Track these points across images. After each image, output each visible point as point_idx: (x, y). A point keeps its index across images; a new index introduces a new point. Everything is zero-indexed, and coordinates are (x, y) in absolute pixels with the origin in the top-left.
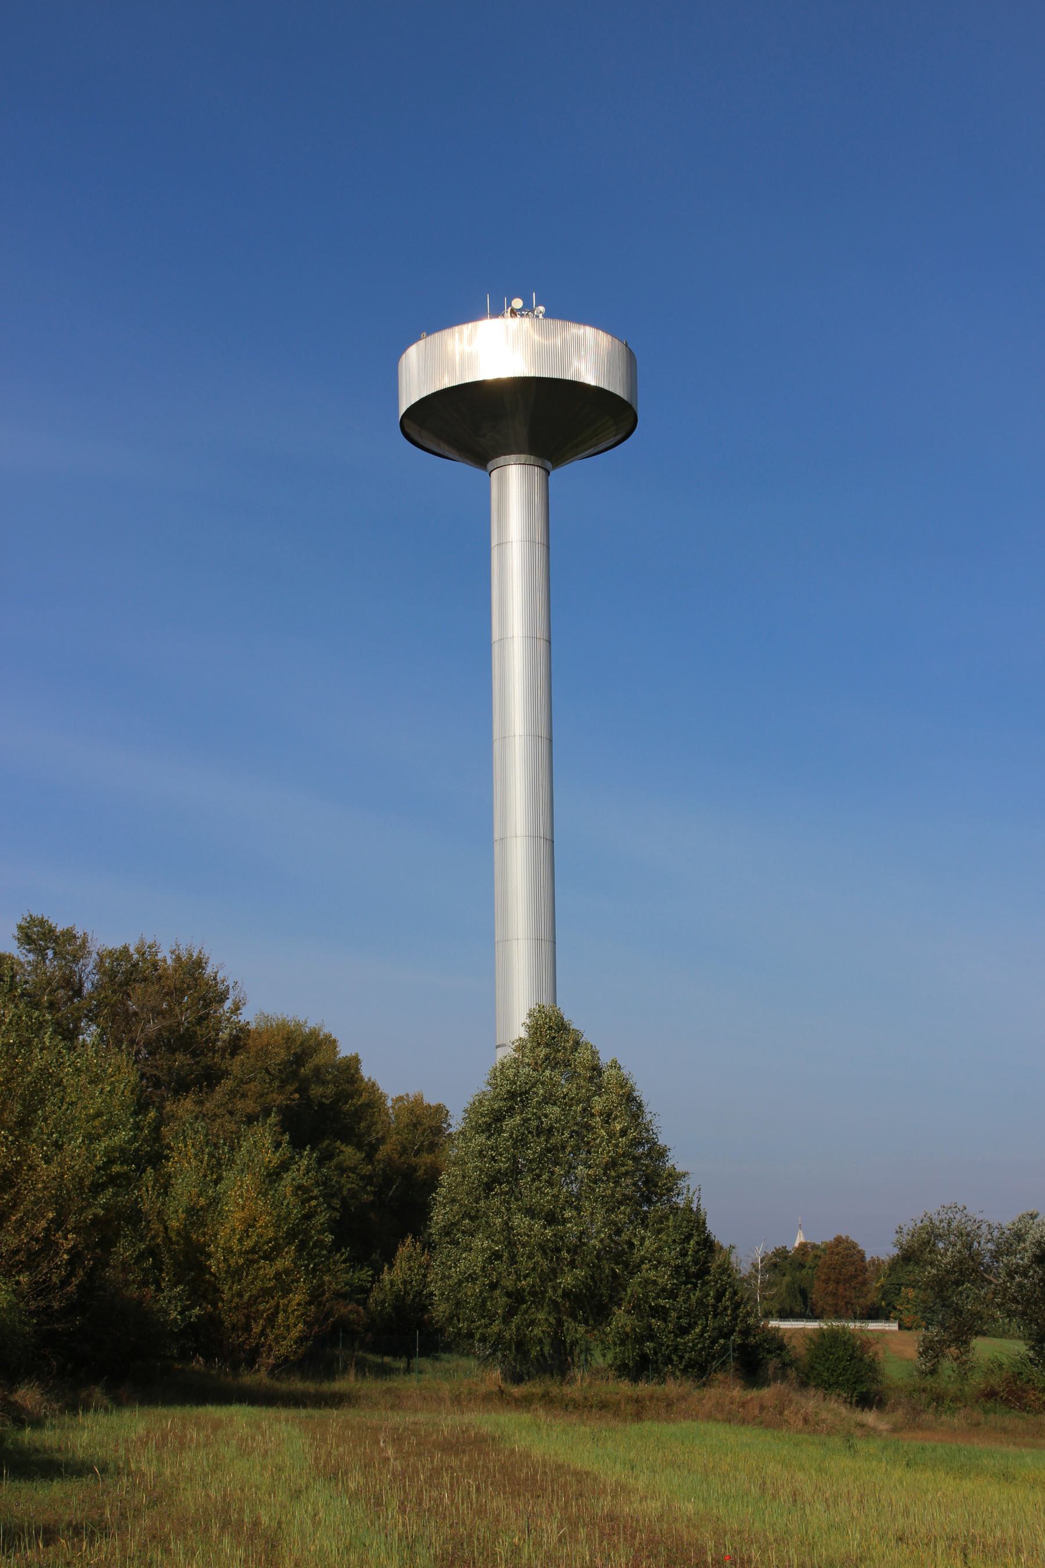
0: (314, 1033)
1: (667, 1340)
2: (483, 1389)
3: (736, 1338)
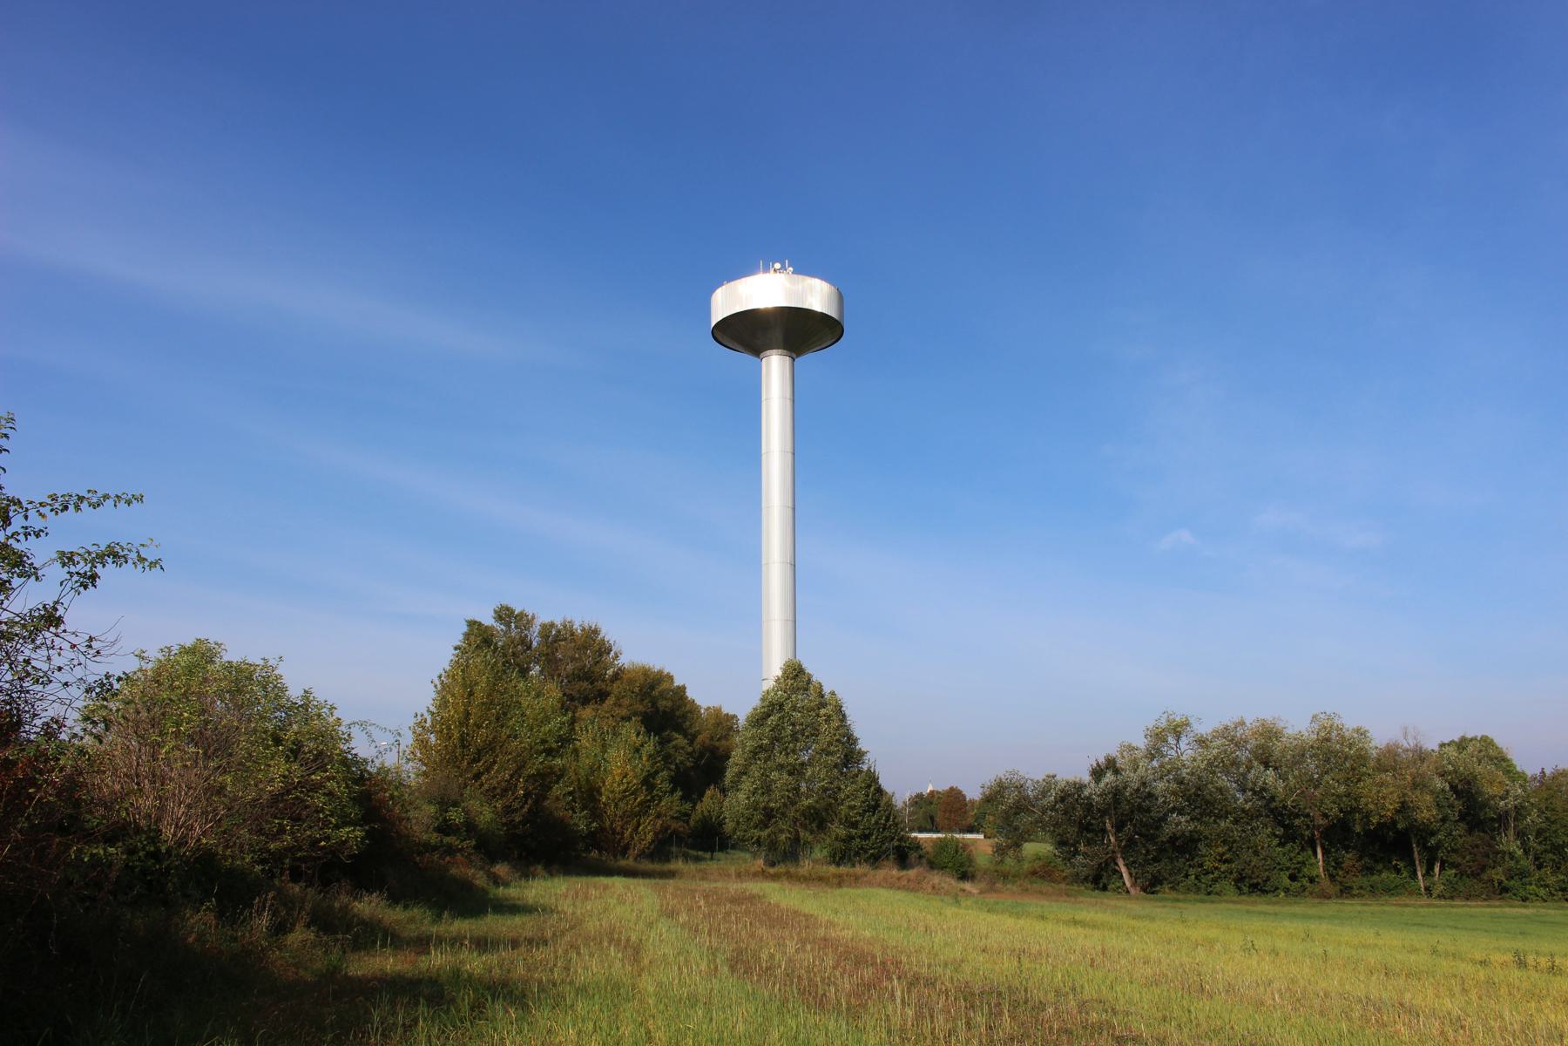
0: (660, 672)
2: (753, 870)
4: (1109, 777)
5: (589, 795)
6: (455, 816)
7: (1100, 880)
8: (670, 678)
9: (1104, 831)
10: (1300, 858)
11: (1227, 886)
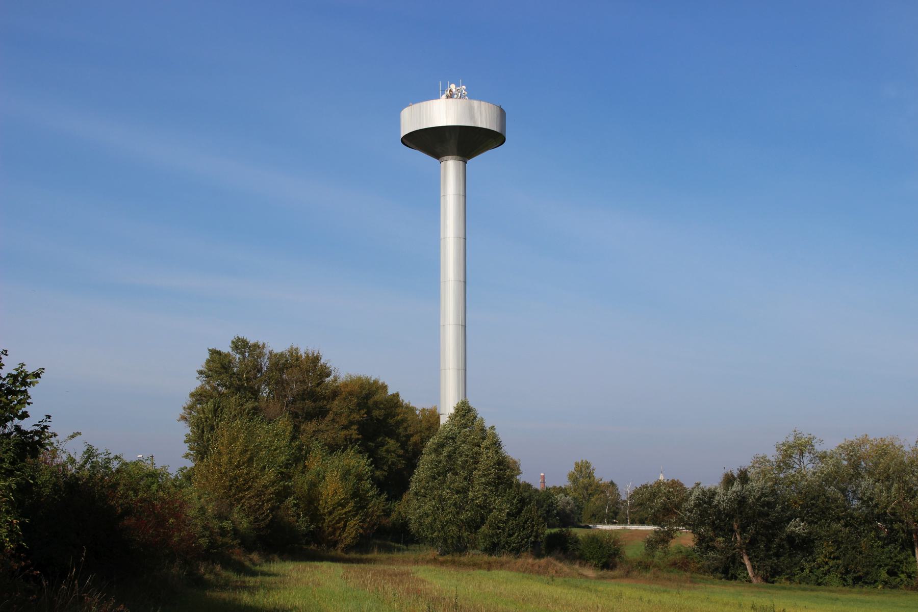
0: (376, 382)
1: (503, 539)
2: (428, 558)
3: (532, 539)
4: (736, 487)
5: (310, 502)
6: (226, 524)
7: (728, 571)
8: (384, 387)
9: (732, 531)
10: (900, 557)
11: (834, 578)
